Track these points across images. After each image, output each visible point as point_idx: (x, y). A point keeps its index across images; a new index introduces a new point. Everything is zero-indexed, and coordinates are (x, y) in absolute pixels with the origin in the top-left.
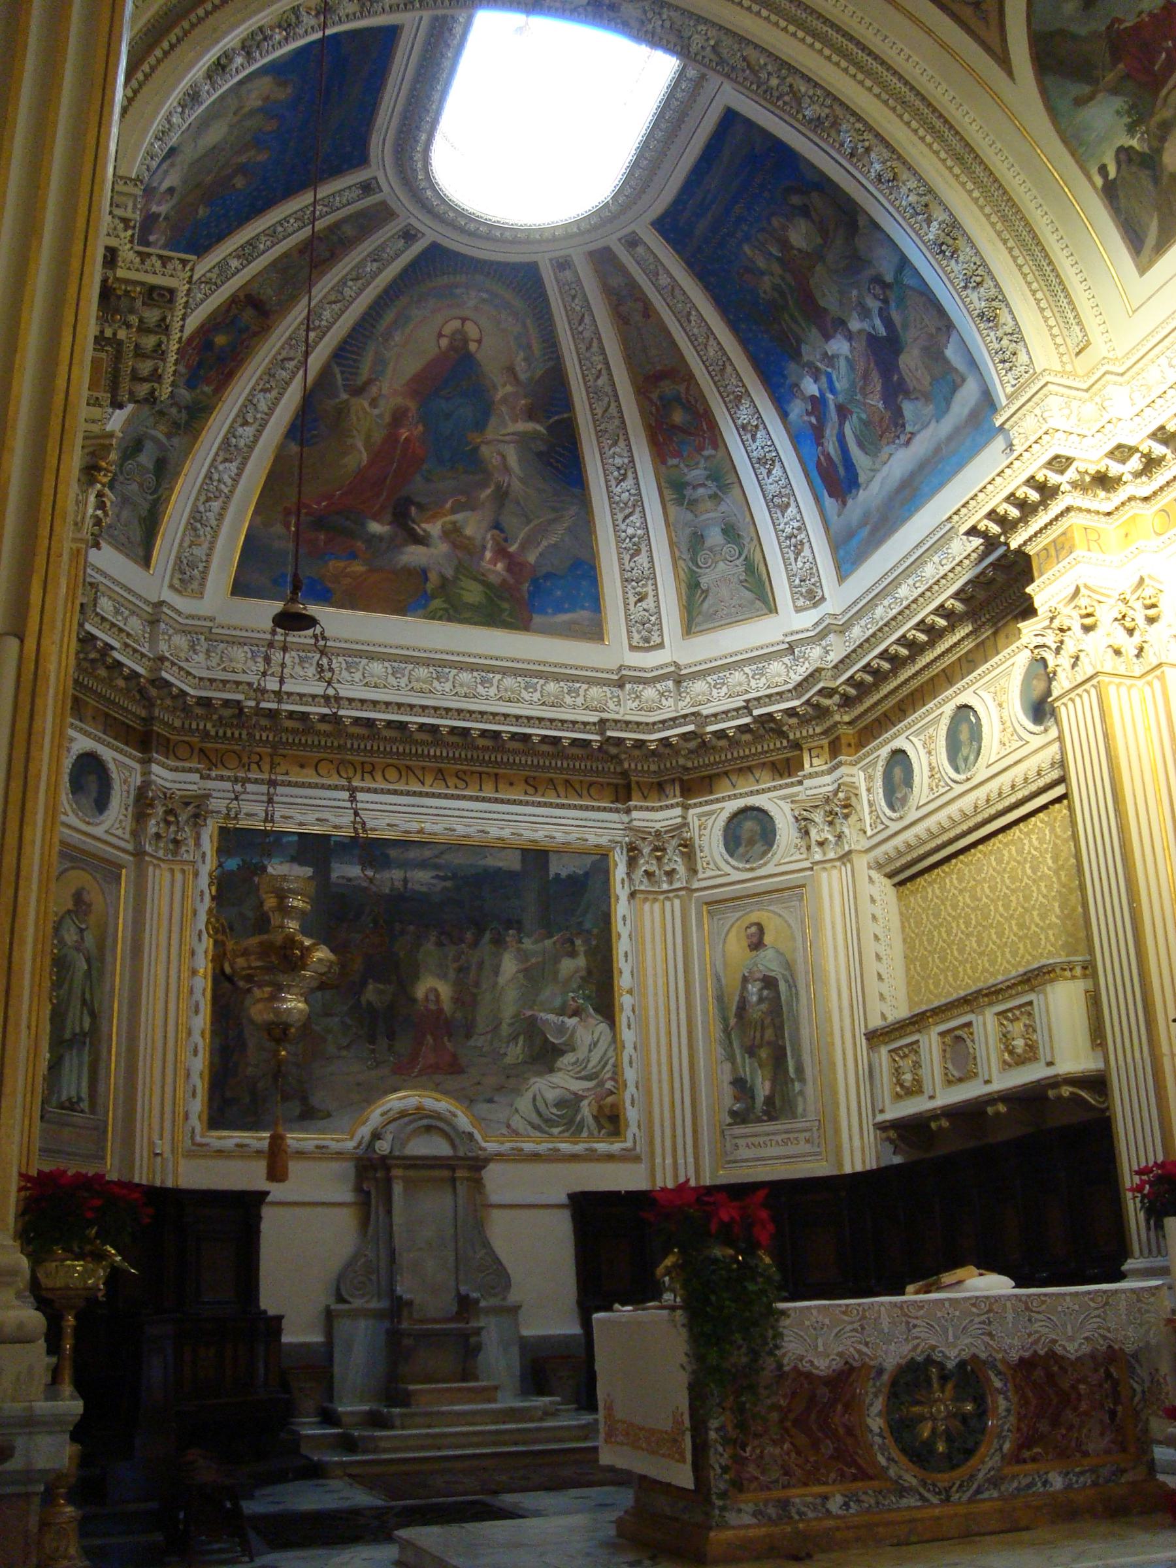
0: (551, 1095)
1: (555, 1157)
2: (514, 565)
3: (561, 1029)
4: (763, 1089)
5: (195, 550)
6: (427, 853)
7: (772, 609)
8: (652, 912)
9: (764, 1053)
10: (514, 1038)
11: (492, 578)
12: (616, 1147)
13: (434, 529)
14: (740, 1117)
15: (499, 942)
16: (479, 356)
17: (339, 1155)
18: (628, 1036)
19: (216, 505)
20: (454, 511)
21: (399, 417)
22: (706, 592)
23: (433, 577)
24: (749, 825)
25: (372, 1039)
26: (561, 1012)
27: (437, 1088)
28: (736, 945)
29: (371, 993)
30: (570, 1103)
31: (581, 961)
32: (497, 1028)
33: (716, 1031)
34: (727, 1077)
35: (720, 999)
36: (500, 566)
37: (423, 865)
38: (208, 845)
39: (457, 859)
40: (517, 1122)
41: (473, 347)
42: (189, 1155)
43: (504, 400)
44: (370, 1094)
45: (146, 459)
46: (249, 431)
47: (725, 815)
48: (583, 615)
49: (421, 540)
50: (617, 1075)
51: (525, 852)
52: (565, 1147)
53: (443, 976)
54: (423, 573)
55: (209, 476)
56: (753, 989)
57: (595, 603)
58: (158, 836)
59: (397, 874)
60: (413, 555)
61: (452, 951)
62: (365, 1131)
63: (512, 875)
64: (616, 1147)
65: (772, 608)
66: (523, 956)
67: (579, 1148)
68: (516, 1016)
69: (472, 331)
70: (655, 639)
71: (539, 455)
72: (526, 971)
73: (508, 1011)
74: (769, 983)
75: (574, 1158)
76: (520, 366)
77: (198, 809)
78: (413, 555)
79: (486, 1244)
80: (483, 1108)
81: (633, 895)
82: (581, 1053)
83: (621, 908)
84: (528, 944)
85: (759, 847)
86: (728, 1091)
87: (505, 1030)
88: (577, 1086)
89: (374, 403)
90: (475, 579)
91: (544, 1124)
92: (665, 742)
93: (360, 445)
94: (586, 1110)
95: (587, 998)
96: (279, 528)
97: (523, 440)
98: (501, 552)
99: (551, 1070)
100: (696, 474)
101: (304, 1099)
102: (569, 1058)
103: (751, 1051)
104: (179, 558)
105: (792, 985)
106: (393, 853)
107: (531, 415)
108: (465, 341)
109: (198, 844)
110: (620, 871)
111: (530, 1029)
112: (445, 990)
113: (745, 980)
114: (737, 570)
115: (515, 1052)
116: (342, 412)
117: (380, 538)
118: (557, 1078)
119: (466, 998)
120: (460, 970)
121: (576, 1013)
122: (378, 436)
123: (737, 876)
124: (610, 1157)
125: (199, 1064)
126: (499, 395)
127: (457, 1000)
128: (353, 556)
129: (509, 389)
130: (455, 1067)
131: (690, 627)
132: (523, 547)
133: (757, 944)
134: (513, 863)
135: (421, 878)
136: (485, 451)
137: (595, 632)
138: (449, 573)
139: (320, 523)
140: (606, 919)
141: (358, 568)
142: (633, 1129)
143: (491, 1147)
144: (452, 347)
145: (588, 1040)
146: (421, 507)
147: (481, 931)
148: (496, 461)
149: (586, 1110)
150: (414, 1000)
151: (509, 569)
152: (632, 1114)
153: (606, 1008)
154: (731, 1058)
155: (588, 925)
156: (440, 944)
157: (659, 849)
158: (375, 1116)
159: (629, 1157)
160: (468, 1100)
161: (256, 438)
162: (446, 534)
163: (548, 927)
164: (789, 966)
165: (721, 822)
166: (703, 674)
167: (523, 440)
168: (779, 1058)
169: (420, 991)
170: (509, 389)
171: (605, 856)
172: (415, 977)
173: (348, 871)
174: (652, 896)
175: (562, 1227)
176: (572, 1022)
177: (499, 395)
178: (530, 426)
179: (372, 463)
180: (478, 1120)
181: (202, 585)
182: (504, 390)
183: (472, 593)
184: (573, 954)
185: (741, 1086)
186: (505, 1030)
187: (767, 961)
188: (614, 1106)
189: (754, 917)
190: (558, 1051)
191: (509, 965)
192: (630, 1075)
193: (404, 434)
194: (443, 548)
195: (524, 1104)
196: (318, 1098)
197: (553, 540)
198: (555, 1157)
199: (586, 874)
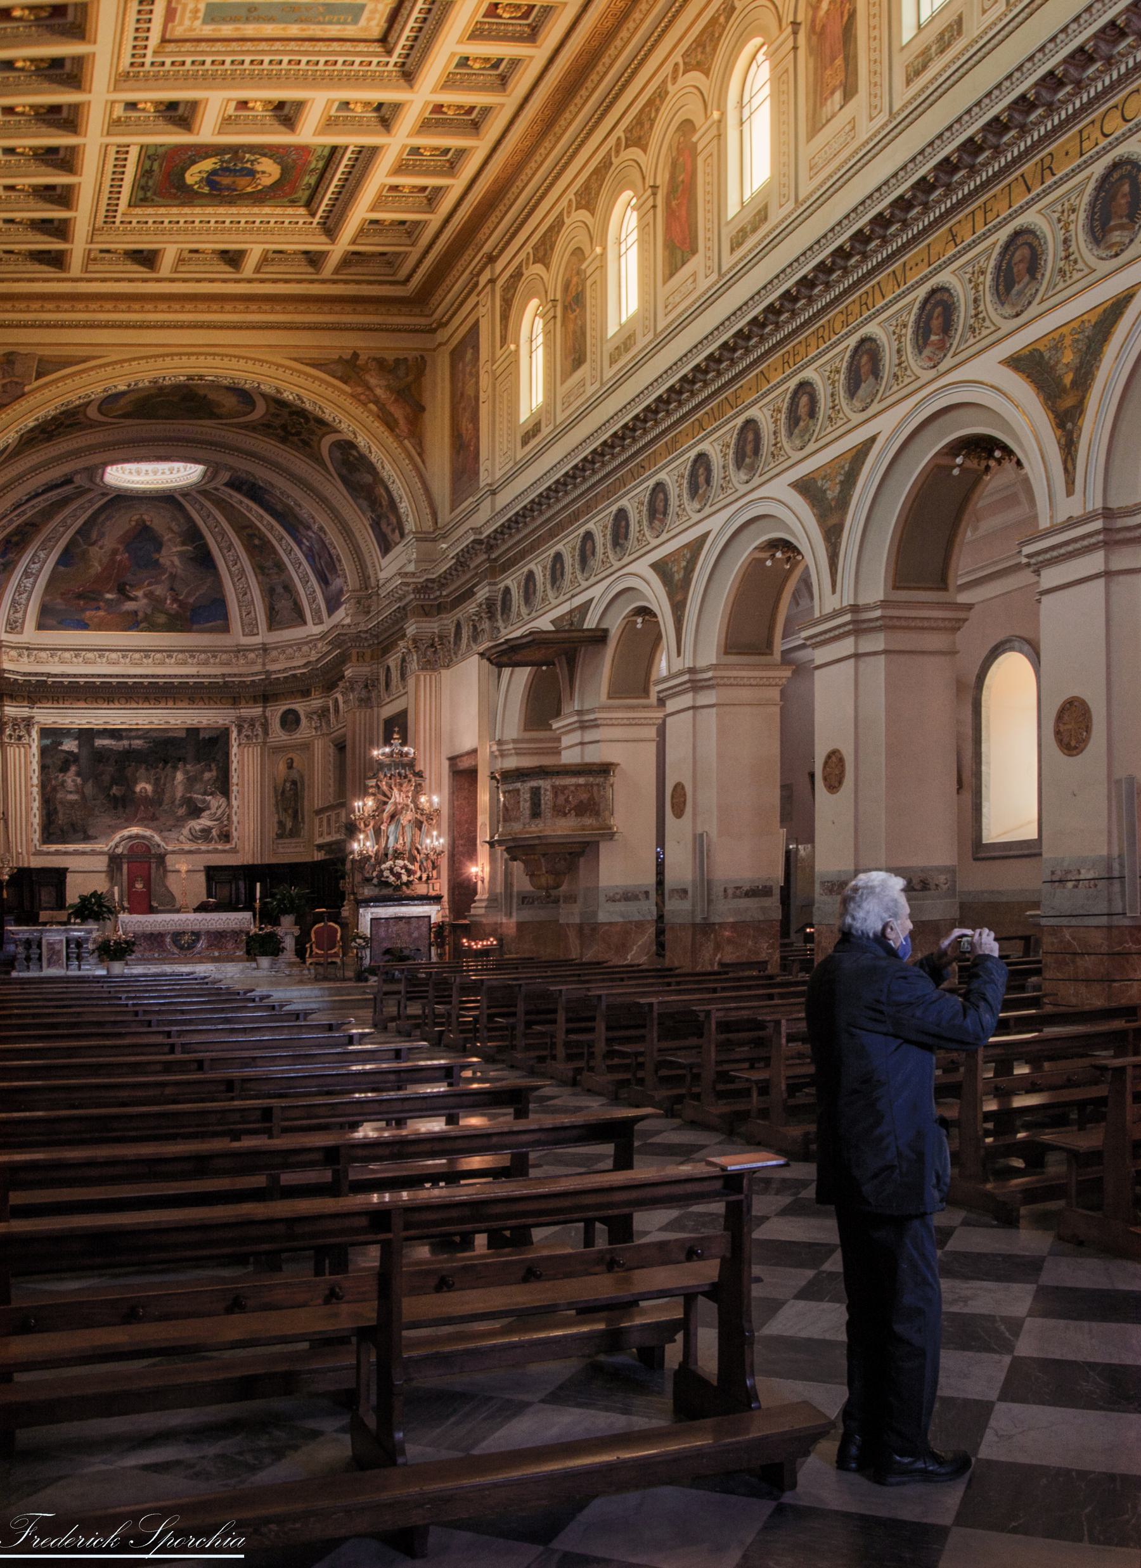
0: (198, 828)
1: (198, 852)
2: (182, 604)
3: (204, 801)
4: (289, 825)
5: (17, 615)
6: (140, 733)
7: (305, 623)
8: (559, 728)
9: (290, 811)
10: (181, 806)
11: (173, 612)
12: (228, 847)
13: (140, 594)
14: (280, 836)
15: (175, 768)
16: (153, 526)
17: (101, 853)
18: (234, 803)
19: (24, 596)
20: (149, 585)
21: (115, 552)
22: (277, 613)
23: (141, 615)
24: (290, 716)
25: (115, 808)
26: (205, 793)
27: (146, 826)
28: (282, 767)
29: (115, 790)
30: (206, 831)
31: (214, 773)
32: (173, 802)
33: (273, 801)
34: (276, 820)
35: (275, 788)
36: (175, 606)
37: (138, 738)
38: (35, 734)
39: (155, 735)
40: (182, 838)
41: (148, 523)
42: (34, 854)
43: (169, 540)
44: (115, 829)
45: (280, 590)
46: (37, 566)
47: (281, 711)
48: (219, 622)
49: (135, 599)
50: (229, 817)
51: (188, 729)
52: (203, 848)
53: (148, 782)
54: (136, 613)
55: (19, 585)
56: (288, 785)
57: (226, 617)
58: (10, 736)
59: (126, 742)
60: (129, 606)
61: (153, 772)
62: (112, 844)
63: (182, 739)
64: (228, 847)
65: (305, 623)
66: (186, 772)
67: (211, 848)
68: (182, 797)
69: (145, 517)
70: (255, 631)
71: (191, 559)
72: (188, 779)
73: (179, 795)
74: (294, 783)
75: (208, 852)
76: (175, 528)
77: (28, 722)
78: (129, 606)
79: (167, 888)
80: (166, 834)
81: (240, 745)
82: (213, 811)
83: (234, 750)
84: (188, 767)
85: (294, 726)
86: (276, 825)
87: (177, 802)
88: (210, 823)
89: (101, 548)
90: (162, 612)
91: (194, 838)
92: (253, 681)
93: (96, 564)
94: (214, 833)
95: (217, 788)
96: (59, 600)
97: (181, 554)
98: (175, 600)
99: (199, 817)
100: (269, 564)
101: (85, 832)
102: (208, 812)
103: (285, 810)
104: (8, 619)
105: (303, 784)
106: (124, 734)
107: (183, 544)
108: (144, 521)
109: (30, 736)
110: (234, 735)
111: (188, 802)
112: (149, 788)
113: (285, 781)
114: (290, 604)
115: (181, 811)
116: (84, 553)
117: (112, 600)
118: (201, 821)
119: (159, 790)
120: (157, 779)
121: (211, 794)
122: (105, 560)
123: (285, 738)
124: (224, 851)
125: (36, 821)
126: (166, 538)
127: (155, 791)
128: (98, 608)
129: (170, 535)
130: (154, 818)
131: (271, 628)
132: (187, 597)
133: (290, 766)
134: (183, 734)
135: (138, 743)
136: (162, 560)
137: (226, 629)
138: (149, 611)
139: (80, 596)
140: (227, 755)
141: (102, 613)
142: (236, 839)
143: (169, 848)
144: (137, 524)
145: (216, 805)
146: (131, 586)
147: (166, 762)
148: (168, 563)
149: (214, 833)
150: (135, 792)
151: (180, 606)
152: (235, 834)
153: (226, 792)
154: (278, 813)
155: (218, 758)
156: (147, 770)
157: (252, 725)
158: (117, 837)
159: (234, 851)
160: (160, 831)
161: (42, 568)
162: (146, 595)
163: (198, 760)
164: (302, 777)
165: (279, 714)
166: (276, 648)
167: (181, 554)
168: (296, 813)
169: (138, 789)
170: (170, 535)
171: (227, 729)
172: (136, 783)
173: (99, 742)
174: (248, 745)
175: (201, 878)
176: (208, 798)
177: (166, 538)
178: (184, 548)
179: (104, 570)
180: (164, 839)
181: (22, 628)
182: (167, 537)
183: (161, 619)
184: (210, 770)
185: (281, 824)
186: (177, 802)
187: (294, 775)
188: (228, 831)
189: (290, 756)
190: (203, 810)
191: (179, 776)
192: (235, 819)
193: (118, 558)
194: (145, 601)
195: (186, 831)
196: (91, 832)
197: (201, 592)
198: (198, 852)
199: (218, 737)
